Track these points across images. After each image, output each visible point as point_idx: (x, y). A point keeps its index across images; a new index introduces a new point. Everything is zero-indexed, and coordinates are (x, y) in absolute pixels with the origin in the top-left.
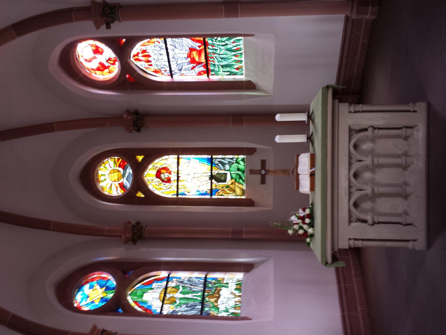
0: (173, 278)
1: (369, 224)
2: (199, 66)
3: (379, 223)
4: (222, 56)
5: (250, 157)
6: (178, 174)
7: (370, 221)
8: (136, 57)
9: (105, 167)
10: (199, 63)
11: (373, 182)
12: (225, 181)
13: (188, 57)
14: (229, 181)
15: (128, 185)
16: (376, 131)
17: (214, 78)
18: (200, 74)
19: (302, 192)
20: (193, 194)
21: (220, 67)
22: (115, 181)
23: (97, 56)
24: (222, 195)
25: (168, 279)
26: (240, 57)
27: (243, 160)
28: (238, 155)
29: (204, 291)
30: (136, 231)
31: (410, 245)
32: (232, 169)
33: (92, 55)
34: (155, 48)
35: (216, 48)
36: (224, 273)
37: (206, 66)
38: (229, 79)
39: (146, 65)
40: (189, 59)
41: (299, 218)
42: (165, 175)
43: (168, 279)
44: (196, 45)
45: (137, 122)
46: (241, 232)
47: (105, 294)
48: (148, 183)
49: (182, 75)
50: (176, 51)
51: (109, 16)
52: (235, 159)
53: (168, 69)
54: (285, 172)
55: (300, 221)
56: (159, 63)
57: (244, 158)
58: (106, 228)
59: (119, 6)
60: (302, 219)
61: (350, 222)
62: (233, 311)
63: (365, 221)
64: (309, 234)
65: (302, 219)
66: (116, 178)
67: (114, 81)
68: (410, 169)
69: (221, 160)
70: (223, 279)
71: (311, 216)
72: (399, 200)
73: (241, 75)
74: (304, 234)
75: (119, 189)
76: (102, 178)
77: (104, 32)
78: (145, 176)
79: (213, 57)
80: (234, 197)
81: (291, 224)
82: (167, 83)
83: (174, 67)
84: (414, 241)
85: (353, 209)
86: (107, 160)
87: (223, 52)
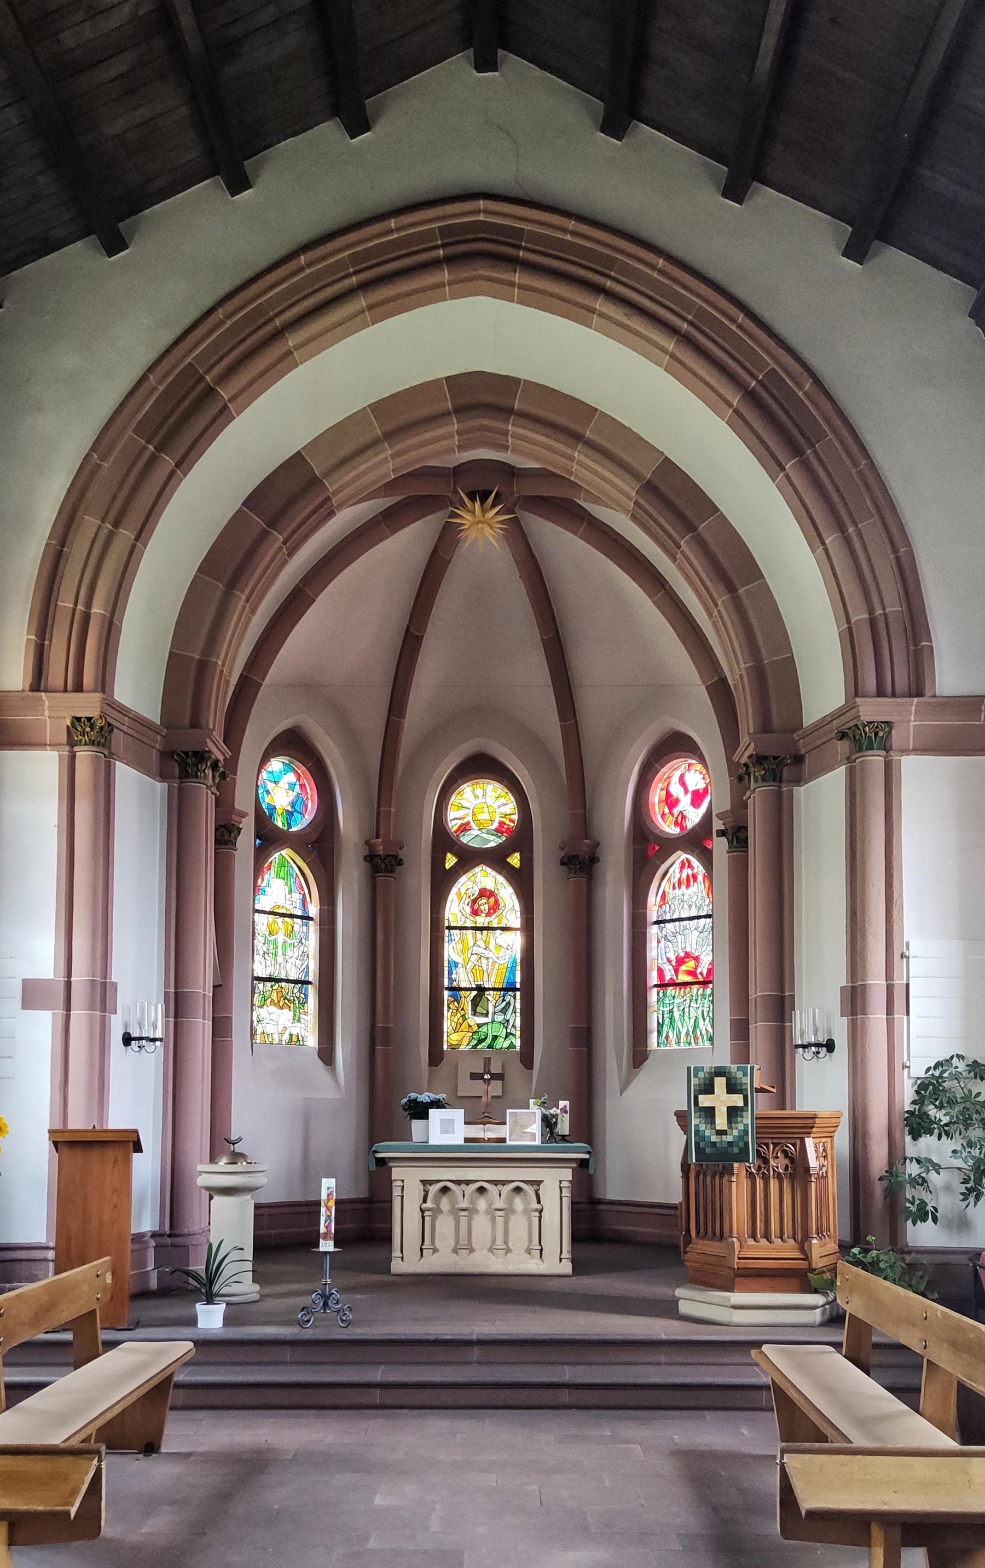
0: (307, 925)
2: (673, 972)
3: (423, 1217)
4: (687, 1010)
7: (424, 1206)
8: (687, 865)
10: (676, 971)
15: (465, 839)
16: (537, 1214)
17: (653, 995)
18: (661, 972)
20: (450, 952)
21: (671, 1007)
23: (689, 796)
24: (449, 1008)
27: (512, 1046)
28: (521, 1037)
29: (288, 981)
30: (387, 861)
31: (396, 1253)
33: (691, 788)
34: (700, 898)
35: (699, 1001)
37: (673, 984)
42: (484, 905)
44: (703, 969)
45: (577, 862)
46: (387, 1042)
48: (470, 874)
50: (696, 933)
52: (513, 1031)
53: (668, 917)
56: (676, 902)
57: (515, 1047)
58: (392, 810)
62: (259, 1032)
63: (425, 1201)
68: (490, 1254)
69: (512, 1005)
70: (306, 1013)
72: (451, 1243)
73: (658, 1043)
75: (459, 822)
76: (479, 792)
77: (718, 825)
78: (484, 868)
79: (685, 995)
80: (445, 1029)
84: (402, 1258)
87: (693, 1014)
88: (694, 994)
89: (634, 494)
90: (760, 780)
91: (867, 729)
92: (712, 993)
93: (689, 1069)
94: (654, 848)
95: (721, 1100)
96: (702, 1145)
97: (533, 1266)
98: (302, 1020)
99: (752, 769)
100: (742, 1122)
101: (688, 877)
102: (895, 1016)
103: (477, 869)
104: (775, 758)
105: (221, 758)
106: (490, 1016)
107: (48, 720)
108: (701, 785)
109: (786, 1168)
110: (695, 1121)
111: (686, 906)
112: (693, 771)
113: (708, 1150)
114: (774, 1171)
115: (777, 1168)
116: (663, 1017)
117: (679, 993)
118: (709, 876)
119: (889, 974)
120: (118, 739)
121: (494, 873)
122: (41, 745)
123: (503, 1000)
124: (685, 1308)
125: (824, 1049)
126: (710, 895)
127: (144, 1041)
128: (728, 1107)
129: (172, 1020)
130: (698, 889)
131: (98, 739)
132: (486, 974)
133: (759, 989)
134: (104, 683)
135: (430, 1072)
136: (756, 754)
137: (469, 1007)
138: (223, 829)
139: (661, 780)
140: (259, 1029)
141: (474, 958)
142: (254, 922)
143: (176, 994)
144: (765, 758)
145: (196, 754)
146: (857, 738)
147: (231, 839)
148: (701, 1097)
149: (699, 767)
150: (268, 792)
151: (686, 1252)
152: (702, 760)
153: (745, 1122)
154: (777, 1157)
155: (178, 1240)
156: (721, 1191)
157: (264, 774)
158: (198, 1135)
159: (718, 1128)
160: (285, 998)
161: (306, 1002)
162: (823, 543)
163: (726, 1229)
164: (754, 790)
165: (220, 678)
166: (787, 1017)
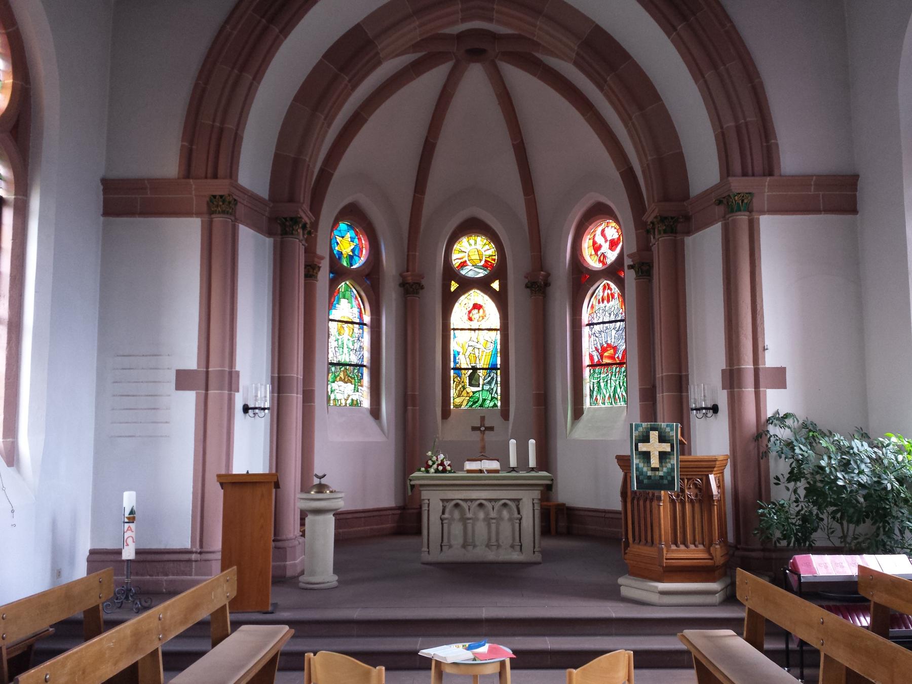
0: (363, 329)
1: (441, 516)
2: (599, 356)
4: (609, 381)
5: (499, 414)
6: (479, 329)
8: (607, 287)
9: (485, 244)
11: (475, 519)
12: (471, 385)
13: (608, 344)
14: (471, 389)
16: (518, 521)
17: (587, 372)
18: (591, 357)
19: (465, 463)
20: (454, 346)
21: (599, 379)
22: (469, 256)
23: (608, 243)
24: (454, 381)
25: (361, 324)
26: (608, 402)
27: (495, 405)
29: (350, 365)
30: (414, 287)
31: (425, 549)
32: (485, 393)
33: (609, 238)
34: (616, 308)
35: (617, 376)
36: (369, 386)
37: (600, 365)
38: (586, 390)
39: (600, 297)
40: (605, 345)
41: (442, 461)
43: (361, 324)
44: (619, 354)
45: (536, 286)
46: (414, 405)
47: (345, 256)
49: (590, 337)
50: (614, 332)
51: (640, 269)
52: (496, 396)
54: (483, 448)
55: (439, 462)
56: (601, 311)
57: (497, 406)
58: (417, 254)
59: (650, 280)
60: (442, 464)
61: (443, 500)
63: (443, 513)
64: (429, 469)
65: (442, 464)
66: (473, 257)
67: (582, 261)
68: (487, 549)
69: (495, 379)
70: (362, 386)
71: (444, 471)
72: (460, 541)
73: (590, 403)
74: (429, 465)
75: (460, 261)
76: (472, 242)
77: (628, 262)
79: (607, 372)
80: (452, 395)
81: (436, 454)
82: (580, 320)
83: (597, 328)
85: (454, 502)
86: (494, 246)
87: (613, 384)
88: (614, 371)
89: (576, 48)
90: (662, 232)
91: (736, 198)
92: (626, 370)
93: (631, 425)
94: (586, 277)
95: (655, 447)
96: (641, 477)
97: (516, 556)
98: (359, 390)
99: (657, 226)
100: (670, 462)
101: (608, 294)
102: (761, 389)
103: (472, 292)
104: (672, 218)
105: (308, 221)
106: (481, 386)
107: (194, 198)
108: (616, 236)
109: (696, 496)
110: (635, 461)
111: (607, 314)
112: (610, 227)
113: (646, 481)
114: (688, 497)
115: (690, 495)
116: (593, 386)
117: (604, 370)
118: (623, 295)
119: (756, 361)
120: (241, 210)
121: (482, 294)
122: (188, 214)
123: (489, 376)
124: (625, 592)
125: (711, 411)
126: (623, 307)
127: (257, 410)
128: (659, 452)
129: (276, 395)
130: (615, 303)
131: (228, 210)
132: (478, 359)
133: (662, 371)
134: (232, 174)
135: (443, 423)
136: (659, 215)
137: (467, 381)
138: (309, 267)
139: (590, 233)
140: (332, 397)
141: (471, 348)
142: (329, 327)
143: (279, 378)
144: (666, 218)
145: (292, 219)
146: (730, 204)
147: (314, 274)
148: (640, 445)
149: (614, 224)
150: (338, 244)
151: (625, 553)
152: (617, 221)
153: (672, 462)
154: (690, 488)
155: (279, 544)
156: (651, 511)
157: (335, 232)
158: (293, 477)
159: (652, 466)
160: (349, 376)
161: (362, 378)
162: (703, 77)
163: (656, 536)
164: (658, 239)
165: (307, 170)
166: (684, 388)
